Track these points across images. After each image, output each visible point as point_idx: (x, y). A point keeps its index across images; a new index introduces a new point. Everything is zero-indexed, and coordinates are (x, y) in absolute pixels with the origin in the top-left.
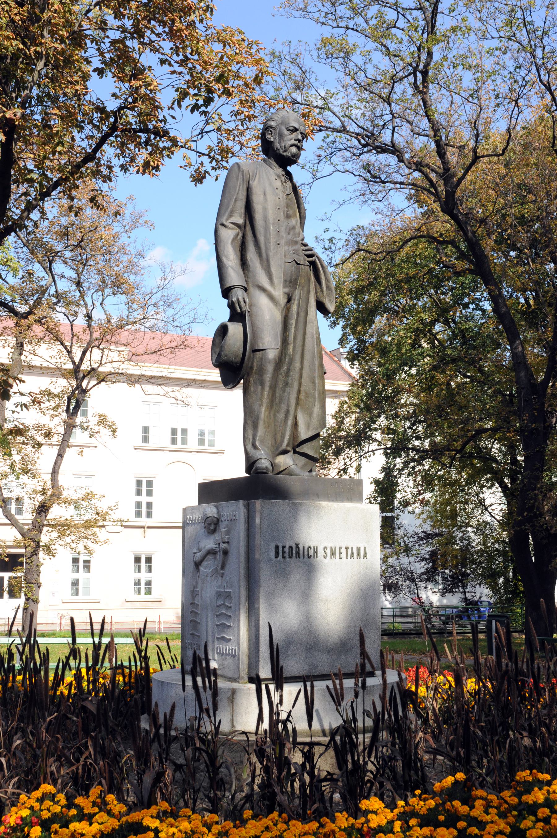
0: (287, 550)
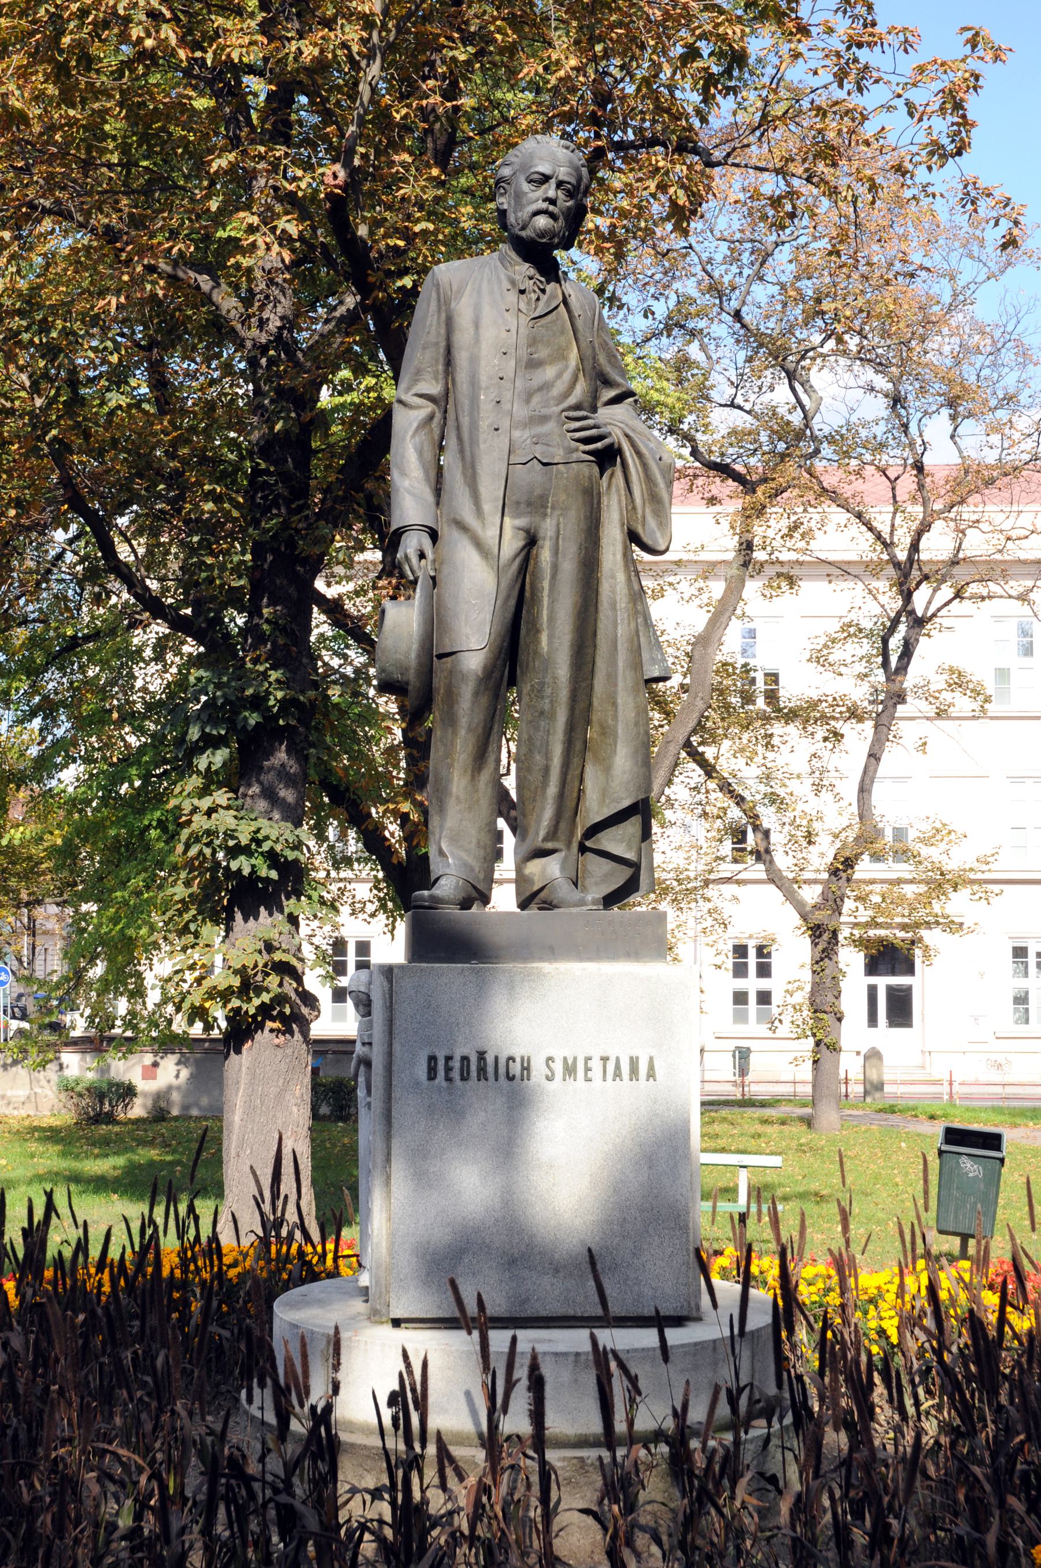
0: (456, 1064)
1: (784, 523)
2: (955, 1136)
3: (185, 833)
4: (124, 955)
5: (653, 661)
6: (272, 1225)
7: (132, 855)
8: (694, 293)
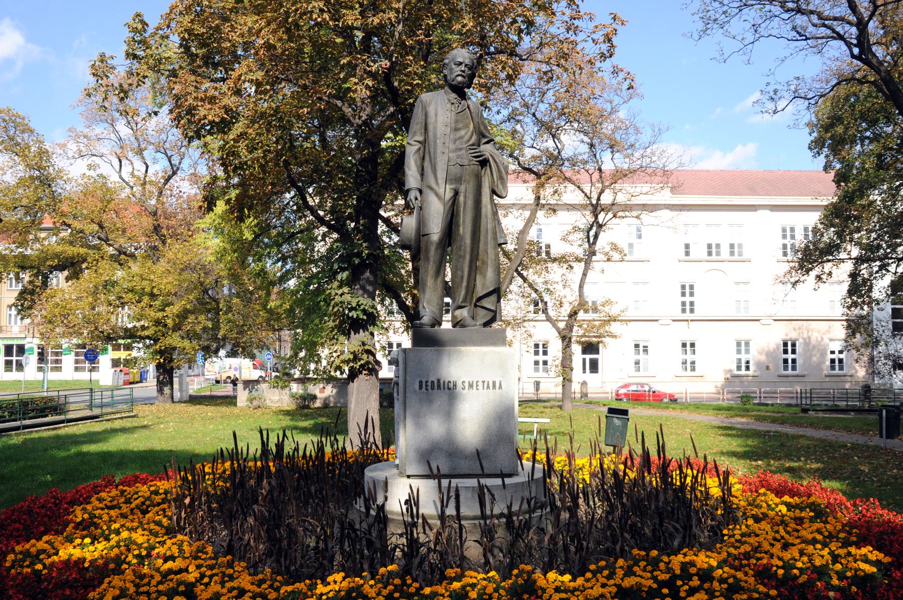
0: (429, 384)
1: (552, 190)
2: (612, 411)
3: (333, 302)
4: (312, 348)
5: (501, 237)
6: (364, 443)
7: (315, 312)
8: (519, 107)
